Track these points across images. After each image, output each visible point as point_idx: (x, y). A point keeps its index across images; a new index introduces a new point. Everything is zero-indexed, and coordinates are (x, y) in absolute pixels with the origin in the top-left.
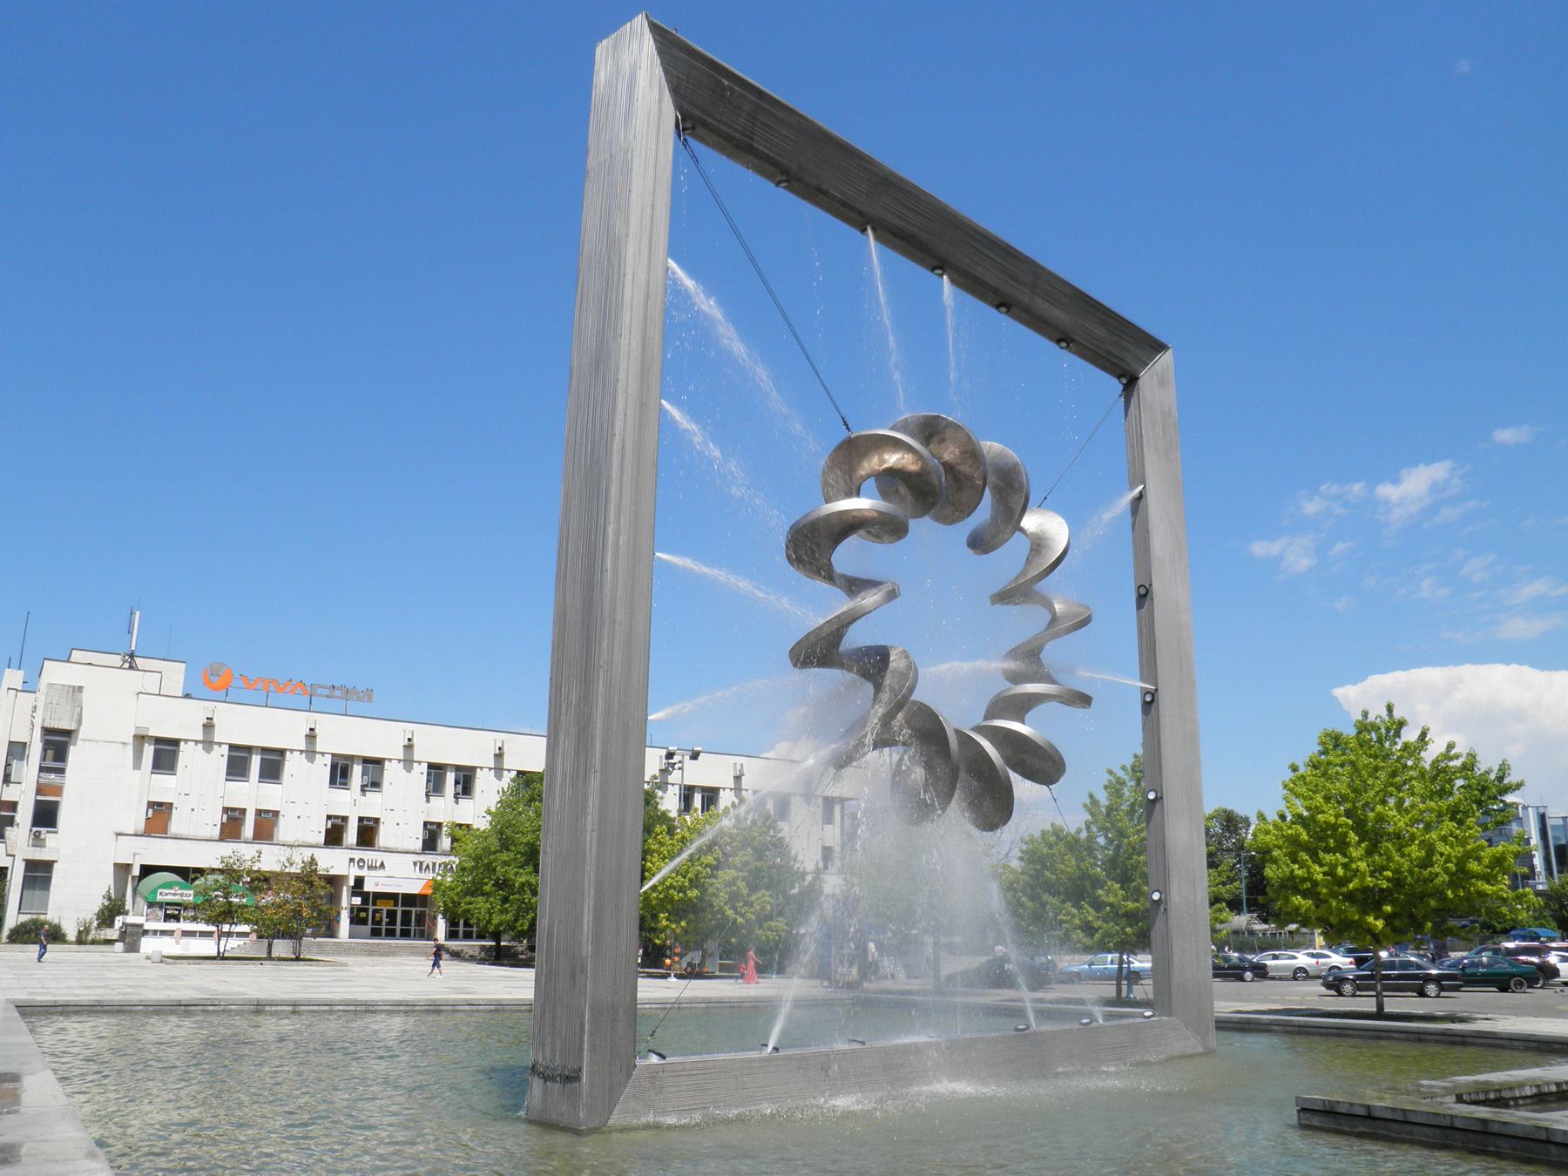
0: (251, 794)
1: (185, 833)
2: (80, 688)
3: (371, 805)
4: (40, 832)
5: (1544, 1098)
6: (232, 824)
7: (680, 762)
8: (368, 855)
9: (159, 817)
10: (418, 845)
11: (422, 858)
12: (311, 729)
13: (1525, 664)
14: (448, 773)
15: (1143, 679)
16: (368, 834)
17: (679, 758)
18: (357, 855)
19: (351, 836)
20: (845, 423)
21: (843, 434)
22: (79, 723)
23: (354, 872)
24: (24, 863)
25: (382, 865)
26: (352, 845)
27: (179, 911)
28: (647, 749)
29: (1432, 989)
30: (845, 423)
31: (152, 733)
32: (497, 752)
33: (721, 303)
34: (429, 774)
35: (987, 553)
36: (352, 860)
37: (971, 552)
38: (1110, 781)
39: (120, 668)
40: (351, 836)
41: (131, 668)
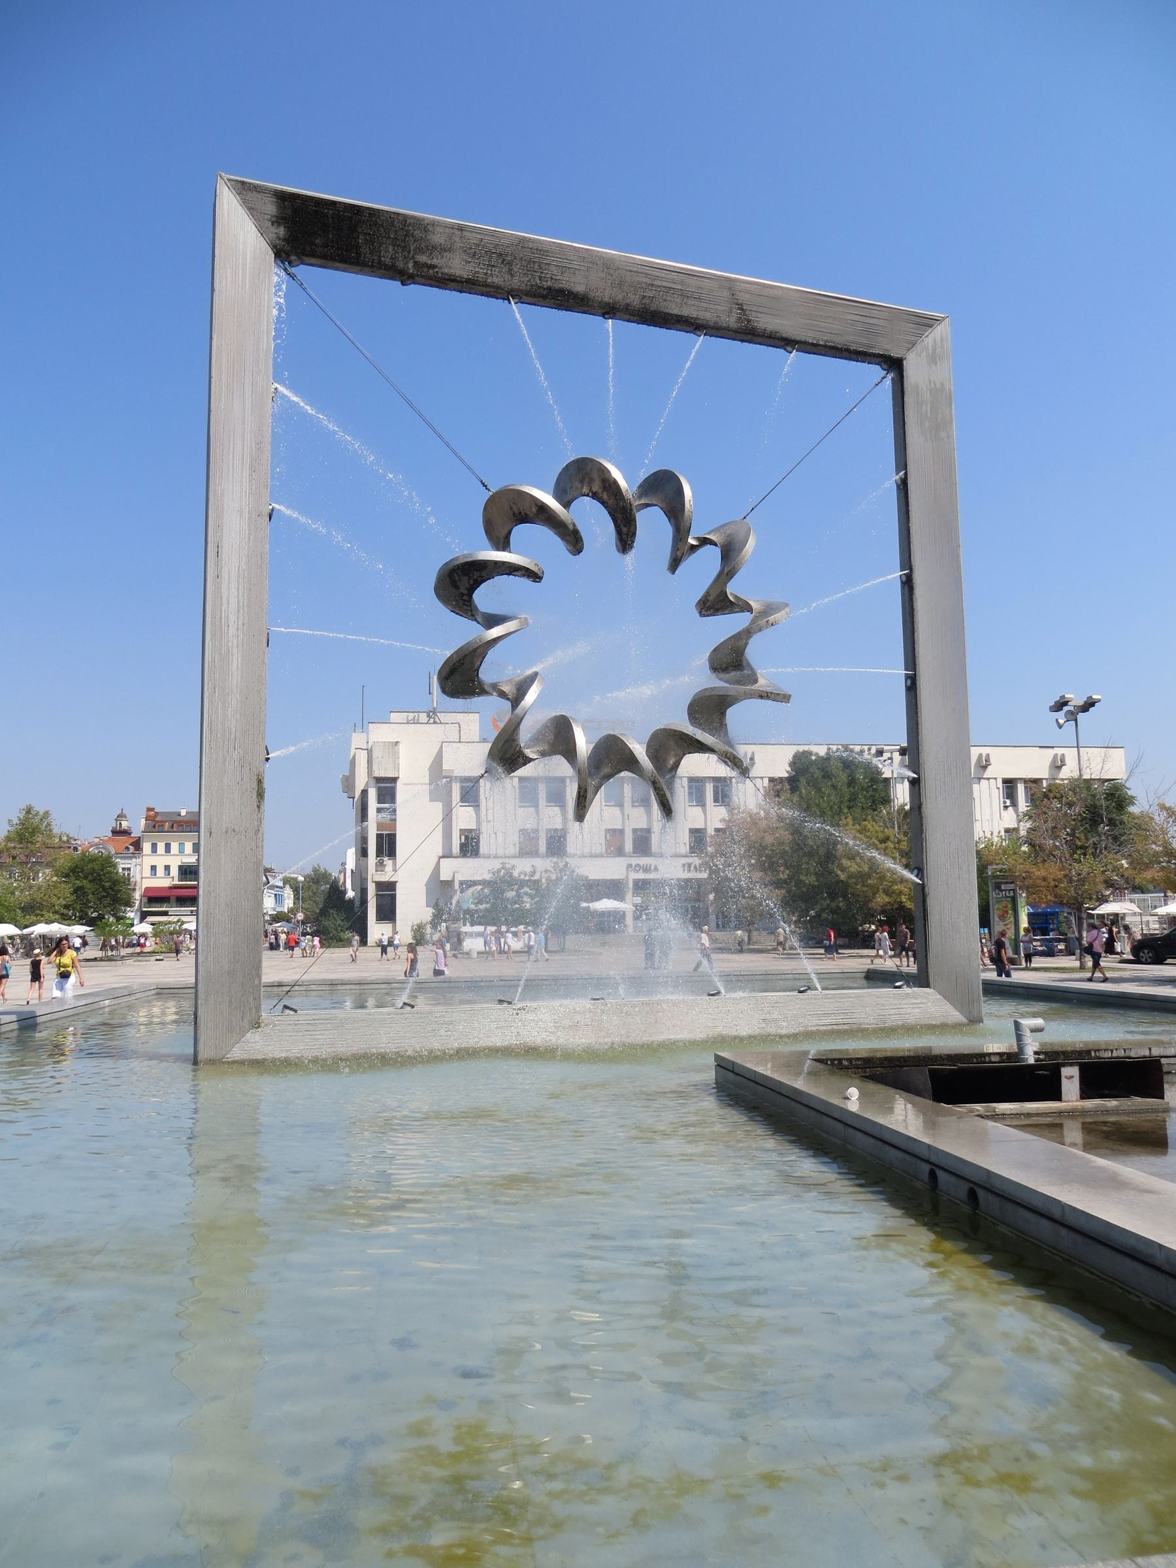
2: (397, 743)
4: (383, 860)
5: (2, 1068)
7: (889, 759)
11: (690, 860)
14: (707, 784)
15: (906, 670)
17: (889, 755)
18: (634, 861)
20: (483, 484)
21: (487, 495)
24: (374, 884)
26: (629, 853)
27: (1014, 890)
28: (972, 748)
30: (483, 484)
31: (456, 774)
33: (301, 397)
34: (690, 787)
36: (629, 866)
38: (37, 814)
39: (428, 723)
41: (435, 722)
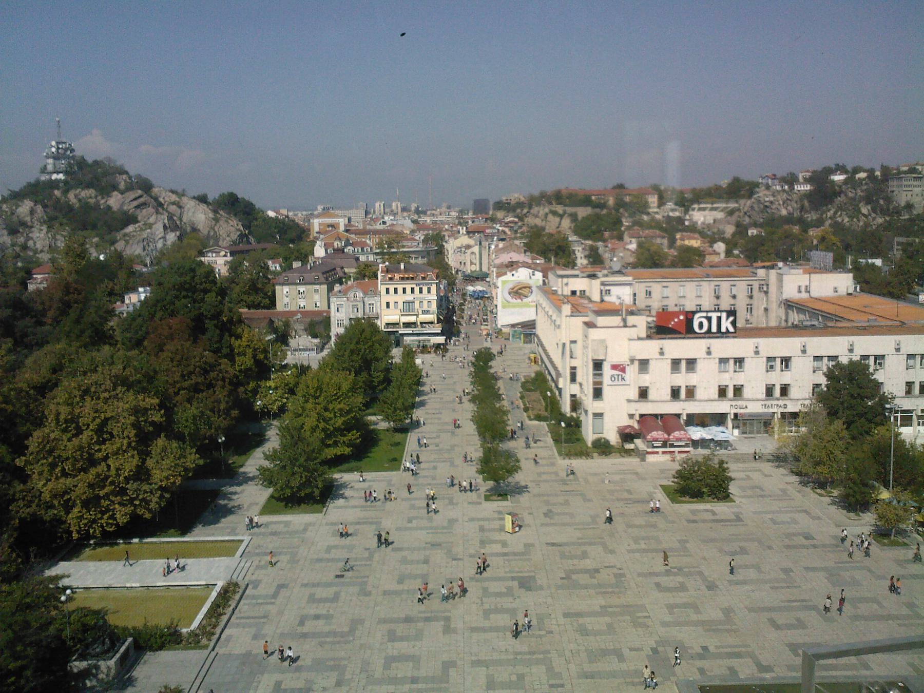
0: (682, 380)
1: (658, 399)
3: (740, 379)
6: (675, 393)
8: (740, 403)
9: (643, 393)
10: (763, 396)
12: (661, 349)
13: (821, 172)
16: (738, 390)
18: (734, 403)
19: (730, 393)
22: (606, 356)
23: (733, 411)
25: (746, 407)
29: (738, 550)
31: (637, 358)
32: (802, 349)
35: (825, 168)
37: (619, 183)
40: (730, 393)
